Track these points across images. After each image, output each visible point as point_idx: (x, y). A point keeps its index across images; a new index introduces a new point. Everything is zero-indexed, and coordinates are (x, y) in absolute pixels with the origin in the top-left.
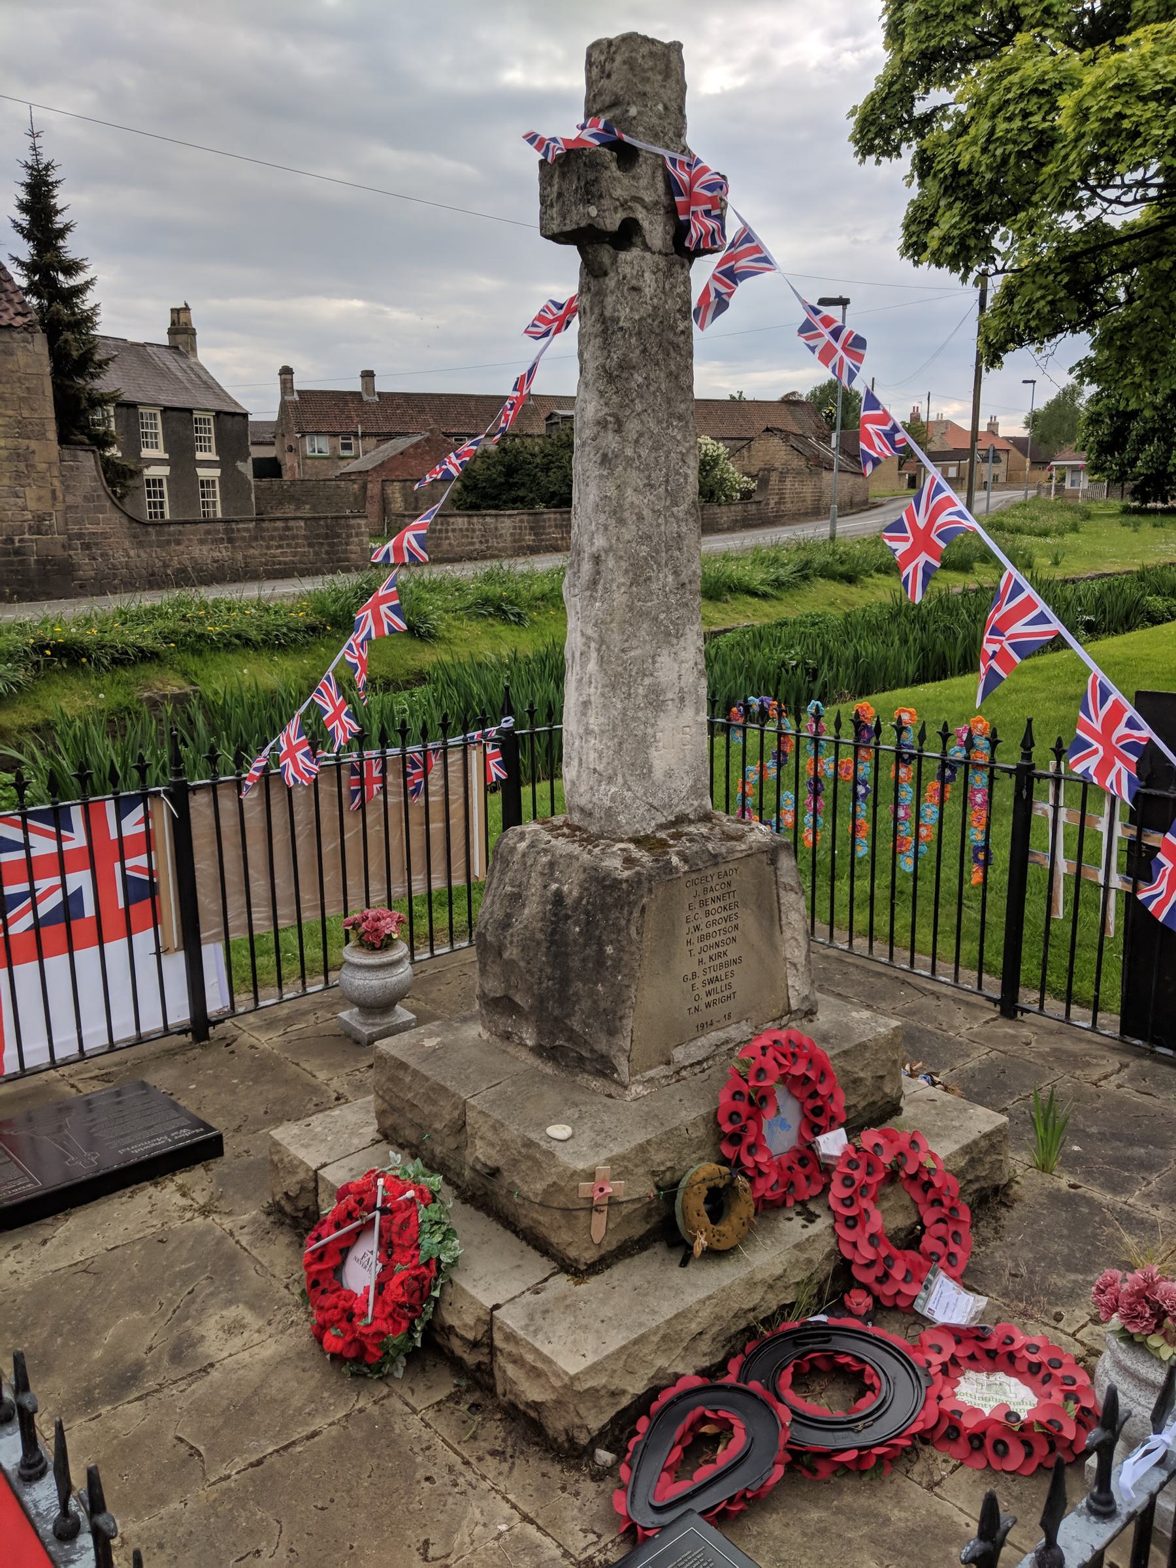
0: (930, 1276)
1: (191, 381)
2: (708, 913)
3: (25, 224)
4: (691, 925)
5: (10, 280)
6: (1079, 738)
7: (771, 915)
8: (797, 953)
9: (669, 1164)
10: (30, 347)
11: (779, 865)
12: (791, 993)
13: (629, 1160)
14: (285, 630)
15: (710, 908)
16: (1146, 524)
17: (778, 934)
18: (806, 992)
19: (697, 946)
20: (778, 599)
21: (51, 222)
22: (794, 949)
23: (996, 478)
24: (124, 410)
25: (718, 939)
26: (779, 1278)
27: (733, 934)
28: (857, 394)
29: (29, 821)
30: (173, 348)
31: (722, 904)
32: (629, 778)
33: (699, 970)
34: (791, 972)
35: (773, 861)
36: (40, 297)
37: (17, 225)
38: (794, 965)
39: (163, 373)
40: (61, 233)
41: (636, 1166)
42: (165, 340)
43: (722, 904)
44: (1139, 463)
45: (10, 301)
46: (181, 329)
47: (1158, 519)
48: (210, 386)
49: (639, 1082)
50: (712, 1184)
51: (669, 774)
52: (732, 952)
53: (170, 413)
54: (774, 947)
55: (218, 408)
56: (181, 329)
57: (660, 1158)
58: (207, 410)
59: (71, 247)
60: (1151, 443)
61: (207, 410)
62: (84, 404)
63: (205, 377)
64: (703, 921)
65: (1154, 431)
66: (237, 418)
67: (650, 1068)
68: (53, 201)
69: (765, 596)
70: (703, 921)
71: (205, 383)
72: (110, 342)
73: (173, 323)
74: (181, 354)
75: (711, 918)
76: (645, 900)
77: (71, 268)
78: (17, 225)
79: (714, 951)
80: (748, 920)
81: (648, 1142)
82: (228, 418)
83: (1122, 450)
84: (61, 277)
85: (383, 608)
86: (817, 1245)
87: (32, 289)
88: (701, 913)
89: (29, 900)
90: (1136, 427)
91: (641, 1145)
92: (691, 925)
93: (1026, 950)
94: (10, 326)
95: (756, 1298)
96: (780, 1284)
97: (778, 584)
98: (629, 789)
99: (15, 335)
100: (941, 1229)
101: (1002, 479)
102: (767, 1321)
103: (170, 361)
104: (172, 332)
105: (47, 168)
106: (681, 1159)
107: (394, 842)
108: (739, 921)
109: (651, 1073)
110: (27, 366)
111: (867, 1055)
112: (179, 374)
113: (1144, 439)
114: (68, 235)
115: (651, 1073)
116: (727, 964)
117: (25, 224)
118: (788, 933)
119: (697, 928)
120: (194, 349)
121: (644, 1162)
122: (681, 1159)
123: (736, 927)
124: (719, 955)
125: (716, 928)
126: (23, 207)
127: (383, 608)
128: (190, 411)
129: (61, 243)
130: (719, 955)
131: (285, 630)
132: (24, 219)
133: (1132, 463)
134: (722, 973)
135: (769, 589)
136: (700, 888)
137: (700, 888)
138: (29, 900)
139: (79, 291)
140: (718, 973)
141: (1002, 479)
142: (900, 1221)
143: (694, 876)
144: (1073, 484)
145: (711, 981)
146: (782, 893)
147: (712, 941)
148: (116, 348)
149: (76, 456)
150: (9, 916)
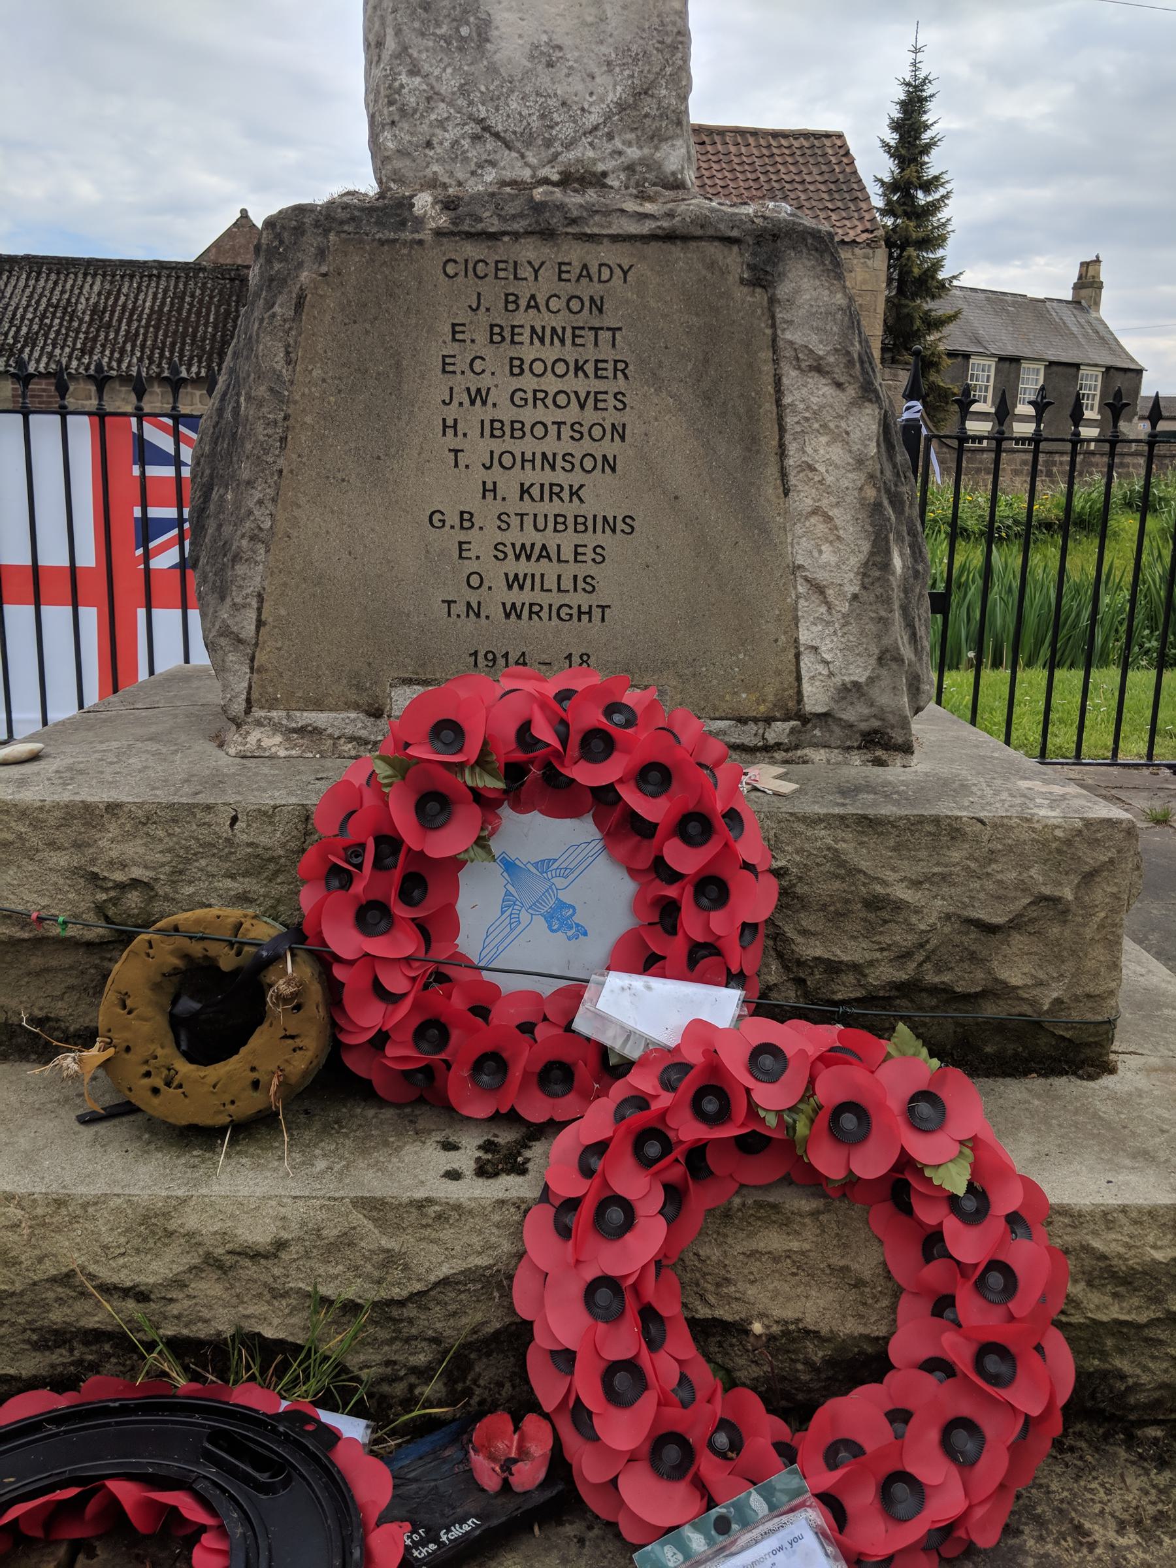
0: (756, 1502)
1: (1086, 335)
2: (517, 367)
3: (892, 143)
4: (460, 382)
5: (867, 199)
7: (753, 440)
8: (828, 555)
9: (137, 872)
10: (870, 263)
11: (783, 290)
12: (808, 663)
13: (37, 825)
14: (1010, 522)
15: (528, 353)
17: (771, 490)
18: (859, 674)
19: (478, 448)
21: (919, 138)
22: (826, 544)
24: (1007, 365)
25: (550, 446)
26: (255, 1255)
27: (609, 448)
29: (182, 429)
30: (1076, 303)
31: (570, 353)
32: (410, 37)
33: (485, 513)
34: (809, 608)
35: (762, 278)
36: (896, 216)
37: (886, 145)
38: (819, 589)
39: (1059, 330)
40: (926, 149)
41: (53, 845)
42: (1068, 295)
43: (570, 353)
45: (861, 219)
46: (1088, 283)
48: (1107, 340)
49: (276, 727)
50: (196, 949)
51: (548, 56)
52: (602, 496)
53: (1054, 368)
54: (762, 534)
55: (1110, 363)
56: (1088, 283)
57: (131, 855)
58: (1096, 365)
59: (934, 163)
61: (1096, 365)
62: (918, 323)
63: (1103, 333)
64: (501, 385)
66: (1130, 375)
67: (318, 705)
68: (925, 118)
70: (501, 385)
71: (1102, 338)
72: (1009, 298)
73: (1080, 278)
74: (1082, 309)
75: (528, 382)
76: (305, 276)
77: (928, 186)
78: (886, 145)
79: (531, 476)
80: (659, 423)
81: (113, 808)
82: (1121, 374)
84: (920, 194)
86: (447, 1234)
87: (889, 211)
88: (495, 359)
89: (175, 532)
91: (87, 807)
92: (460, 382)
94: (854, 241)
95: (154, 1270)
96: (251, 1270)
98: (414, 72)
99: (857, 251)
100: (932, 1397)
102: (203, 1354)
103: (1069, 317)
104: (1077, 287)
105: (923, 83)
106: (178, 875)
108: (627, 417)
109: (319, 718)
110: (864, 282)
111: (956, 855)
112: (1075, 329)
114: (934, 152)
115: (319, 718)
116: (581, 524)
117: (892, 143)
118: (804, 497)
119: (479, 397)
120: (1097, 303)
121: (78, 845)
122: (178, 875)
123: (619, 432)
124: (554, 491)
125: (549, 415)
126: (896, 126)
128: (1077, 366)
129: (926, 159)
130: (554, 491)
131: (1010, 522)
132: (892, 138)
134: (567, 541)
136: (492, 292)
137: (492, 292)
138: (175, 532)
139: (934, 207)
140: (551, 540)
142: (818, 1308)
143: (471, 250)
145: (524, 552)
146: (790, 376)
147: (528, 446)
148: (1014, 304)
149: (896, 375)
150: (152, 545)
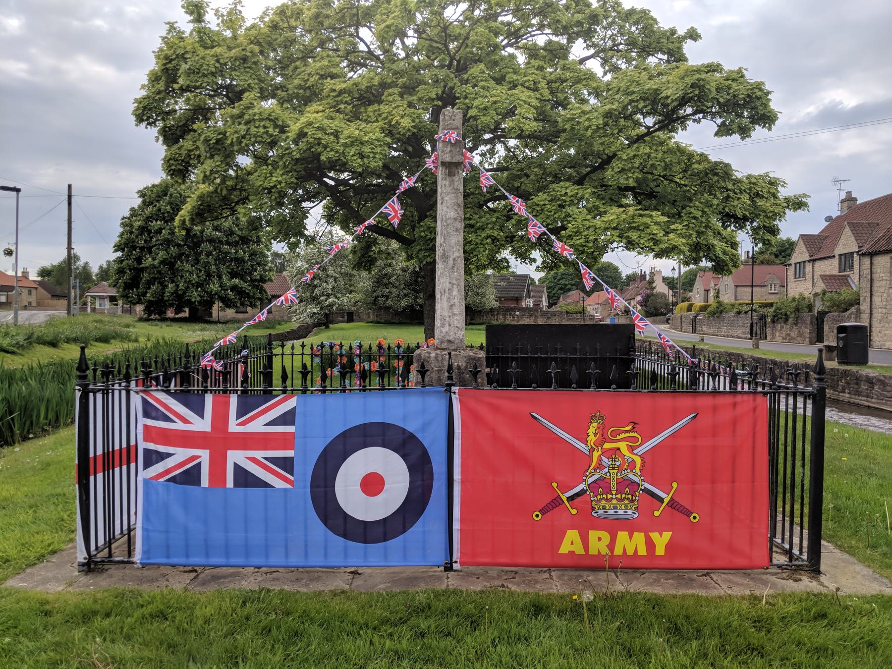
6: (236, 484)
16: (164, 325)
20: (20, 354)
23: (30, 303)
28: (324, 207)
44: (148, 295)
47: (169, 323)
60: (154, 284)
65: (155, 279)
69: (13, 353)
83: (138, 288)
85: (393, 214)
90: (146, 276)
93: (795, 519)
97: (18, 345)
101: (34, 304)
107: (789, 464)
113: (149, 284)
127: (393, 214)
133: (144, 294)
135: (15, 349)
141: (34, 304)
144: (100, 305)
